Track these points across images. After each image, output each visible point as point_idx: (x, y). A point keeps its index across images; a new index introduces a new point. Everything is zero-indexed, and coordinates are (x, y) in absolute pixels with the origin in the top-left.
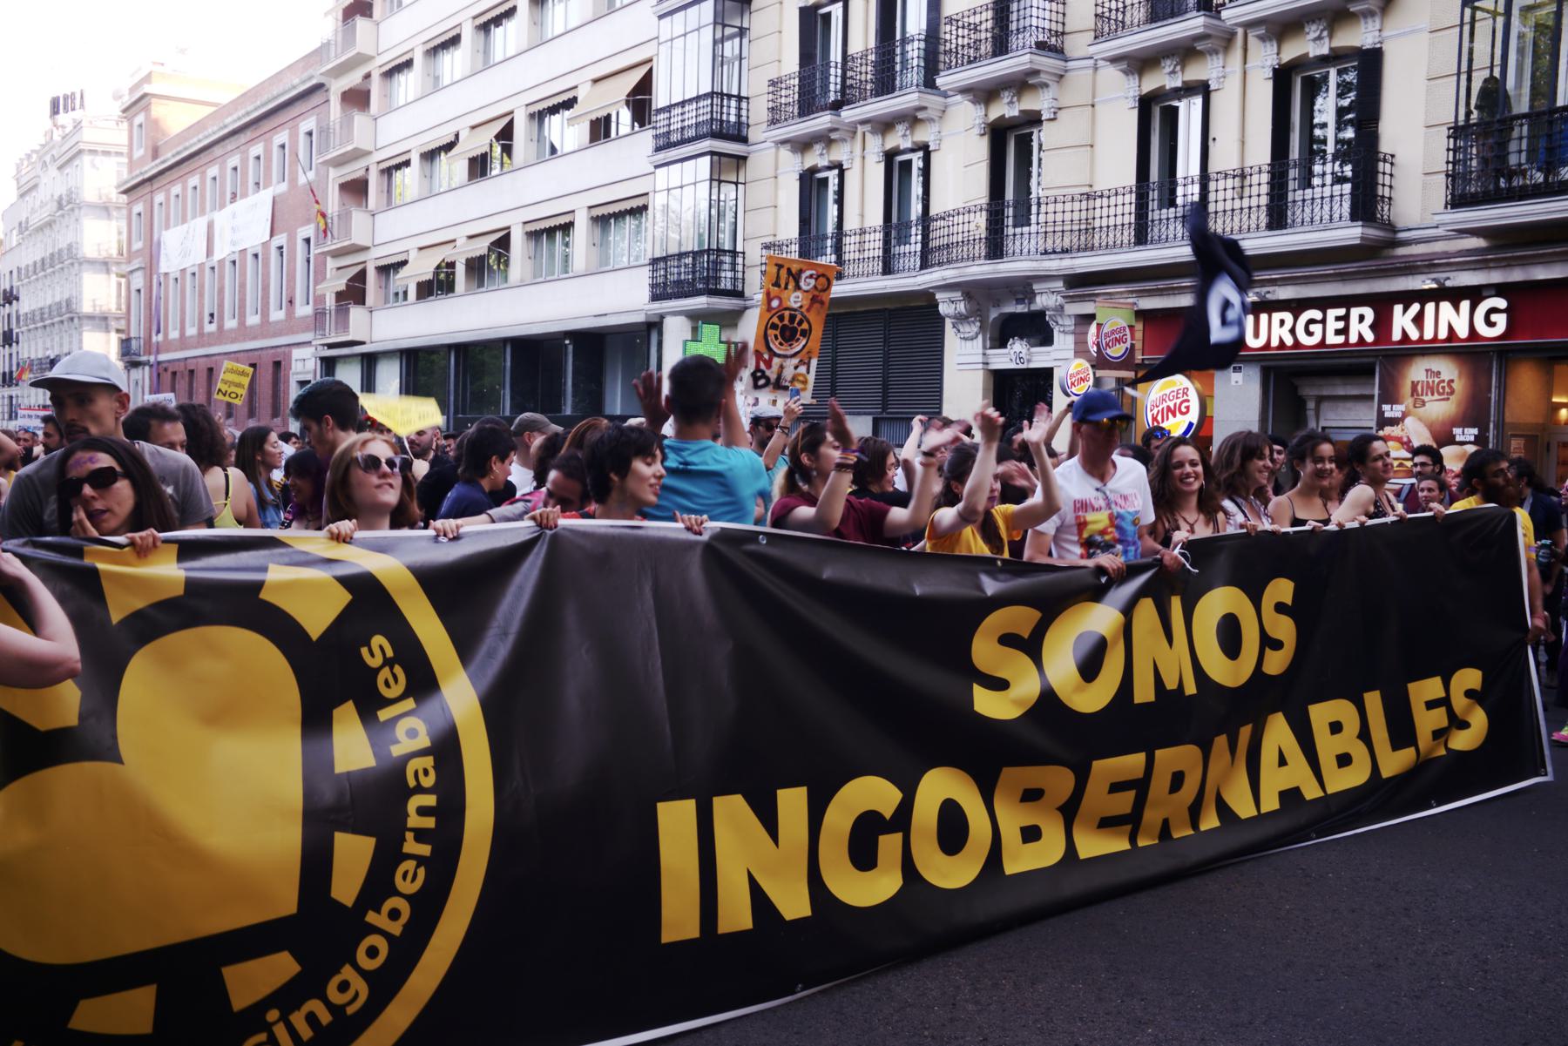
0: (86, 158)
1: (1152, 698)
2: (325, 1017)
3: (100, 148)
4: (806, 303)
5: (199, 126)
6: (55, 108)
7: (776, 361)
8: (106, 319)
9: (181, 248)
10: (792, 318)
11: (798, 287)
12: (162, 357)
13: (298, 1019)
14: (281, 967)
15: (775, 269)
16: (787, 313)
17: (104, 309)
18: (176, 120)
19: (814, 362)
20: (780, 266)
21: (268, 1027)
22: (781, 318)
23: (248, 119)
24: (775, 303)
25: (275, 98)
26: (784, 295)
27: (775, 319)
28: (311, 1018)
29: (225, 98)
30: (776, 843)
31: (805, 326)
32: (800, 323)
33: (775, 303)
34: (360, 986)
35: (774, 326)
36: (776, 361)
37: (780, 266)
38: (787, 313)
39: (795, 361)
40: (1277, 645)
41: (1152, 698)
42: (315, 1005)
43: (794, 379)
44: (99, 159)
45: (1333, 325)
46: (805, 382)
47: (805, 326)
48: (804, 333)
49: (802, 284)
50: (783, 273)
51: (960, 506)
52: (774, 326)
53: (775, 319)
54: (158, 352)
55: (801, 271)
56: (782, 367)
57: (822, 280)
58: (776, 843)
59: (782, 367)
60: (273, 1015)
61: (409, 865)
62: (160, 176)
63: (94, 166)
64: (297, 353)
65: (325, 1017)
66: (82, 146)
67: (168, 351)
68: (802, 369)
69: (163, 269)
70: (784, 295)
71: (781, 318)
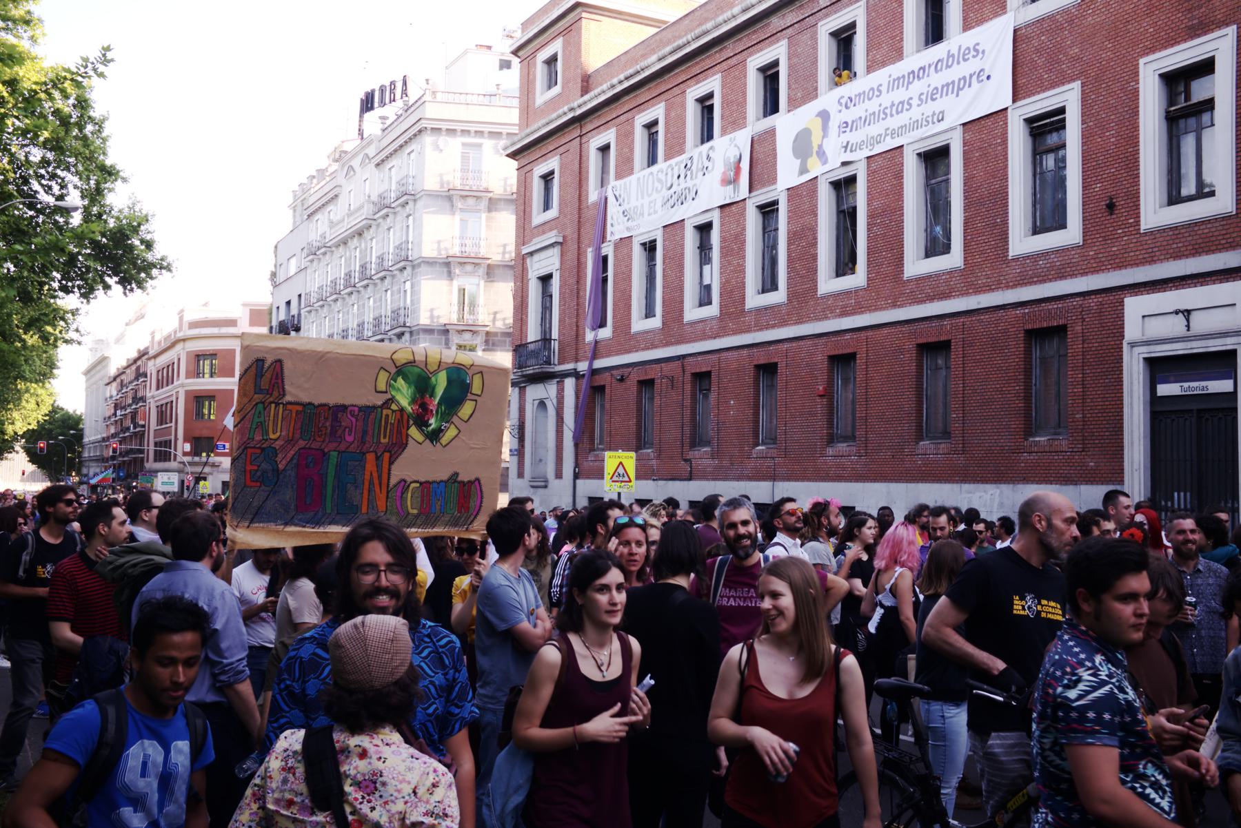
0: (428, 139)
3: (444, 126)
5: (645, 47)
6: (367, 104)
8: (446, 332)
9: (644, 202)
12: (598, 364)
17: (443, 321)
18: (604, 45)
23: (626, 84)
25: (680, 48)
29: (671, 14)
40: (351, 813)
44: (443, 140)
51: (949, 792)
54: (595, 355)
62: (570, 133)
63: (437, 147)
64: (1134, 306)
66: (423, 124)
67: (609, 354)
69: (616, 230)
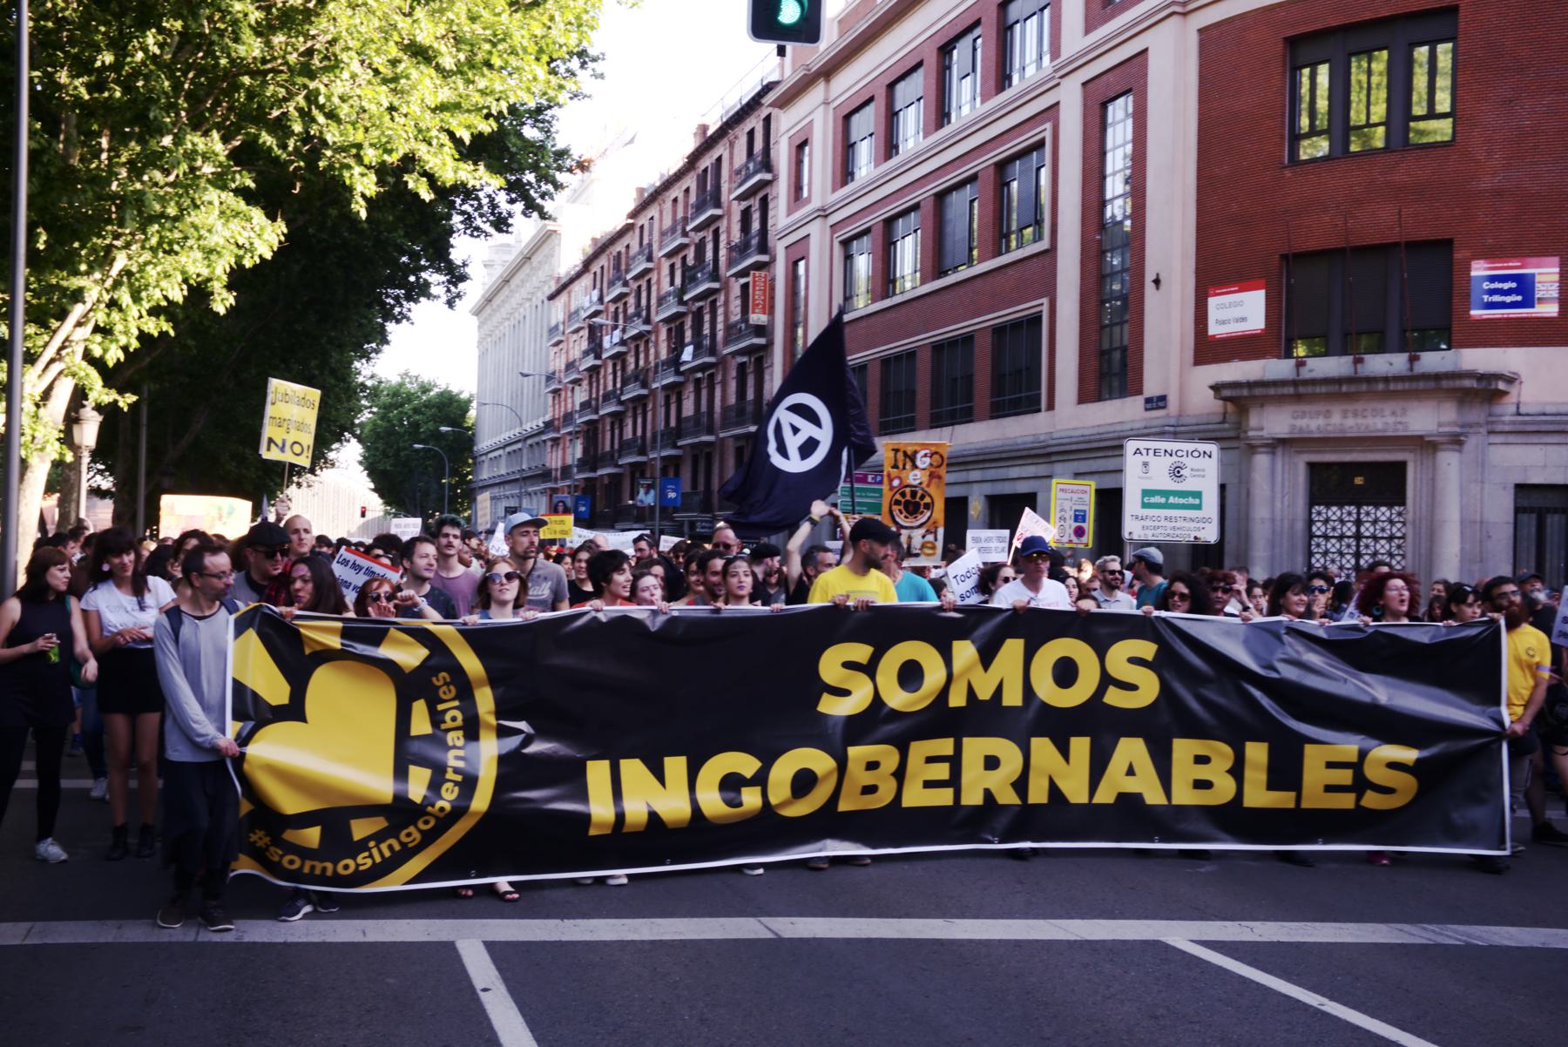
1: (667, 760)
2: (397, 847)
4: (925, 479)
7: (903, 532)
10: (914, 494)
11: (915, 467)
13: (384, 847)
14: (379, 823)
15: (892, 454)
16: (908, 490)
19: (941, 531)
20: (896, 451)
21: (369, 849)
22: (903, 495)
24: (896, 483)
26: (903, 474)
27: (898, 497)
28: (390, 847)
30: (663, 784)
31: (927, 500)
32: (922, 497)
33: (896, 483)
34: (417, 836)
35: (897, 502)
36: (903, 532)
37: (896, 451)
38: (908, 490)
39: (922, 531)
41: (667, 760)
42: (392, 841)
43: (923, 546)
45: (918, 770)
46: (934, 548)
47: (927, 500)
48: (927, 506)
49: (918, 463)
50: (900, 456)
52: (897, 502)
53: (898, 497)
55: (916, 452)
56: (910, 538)
57: (936, 457)
58: (663, 784)
59: (910, 538)
60: (372, 844)
61: (449, 785)
65: (397, 847)
68: (930, 538)
70: (903, 474)
71: (903, 495)
